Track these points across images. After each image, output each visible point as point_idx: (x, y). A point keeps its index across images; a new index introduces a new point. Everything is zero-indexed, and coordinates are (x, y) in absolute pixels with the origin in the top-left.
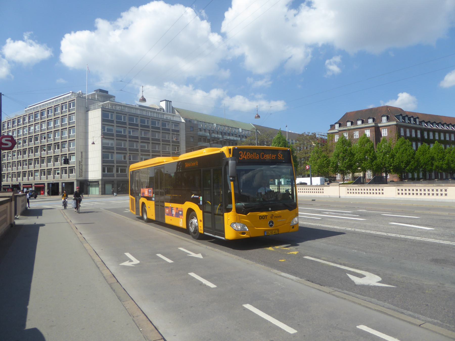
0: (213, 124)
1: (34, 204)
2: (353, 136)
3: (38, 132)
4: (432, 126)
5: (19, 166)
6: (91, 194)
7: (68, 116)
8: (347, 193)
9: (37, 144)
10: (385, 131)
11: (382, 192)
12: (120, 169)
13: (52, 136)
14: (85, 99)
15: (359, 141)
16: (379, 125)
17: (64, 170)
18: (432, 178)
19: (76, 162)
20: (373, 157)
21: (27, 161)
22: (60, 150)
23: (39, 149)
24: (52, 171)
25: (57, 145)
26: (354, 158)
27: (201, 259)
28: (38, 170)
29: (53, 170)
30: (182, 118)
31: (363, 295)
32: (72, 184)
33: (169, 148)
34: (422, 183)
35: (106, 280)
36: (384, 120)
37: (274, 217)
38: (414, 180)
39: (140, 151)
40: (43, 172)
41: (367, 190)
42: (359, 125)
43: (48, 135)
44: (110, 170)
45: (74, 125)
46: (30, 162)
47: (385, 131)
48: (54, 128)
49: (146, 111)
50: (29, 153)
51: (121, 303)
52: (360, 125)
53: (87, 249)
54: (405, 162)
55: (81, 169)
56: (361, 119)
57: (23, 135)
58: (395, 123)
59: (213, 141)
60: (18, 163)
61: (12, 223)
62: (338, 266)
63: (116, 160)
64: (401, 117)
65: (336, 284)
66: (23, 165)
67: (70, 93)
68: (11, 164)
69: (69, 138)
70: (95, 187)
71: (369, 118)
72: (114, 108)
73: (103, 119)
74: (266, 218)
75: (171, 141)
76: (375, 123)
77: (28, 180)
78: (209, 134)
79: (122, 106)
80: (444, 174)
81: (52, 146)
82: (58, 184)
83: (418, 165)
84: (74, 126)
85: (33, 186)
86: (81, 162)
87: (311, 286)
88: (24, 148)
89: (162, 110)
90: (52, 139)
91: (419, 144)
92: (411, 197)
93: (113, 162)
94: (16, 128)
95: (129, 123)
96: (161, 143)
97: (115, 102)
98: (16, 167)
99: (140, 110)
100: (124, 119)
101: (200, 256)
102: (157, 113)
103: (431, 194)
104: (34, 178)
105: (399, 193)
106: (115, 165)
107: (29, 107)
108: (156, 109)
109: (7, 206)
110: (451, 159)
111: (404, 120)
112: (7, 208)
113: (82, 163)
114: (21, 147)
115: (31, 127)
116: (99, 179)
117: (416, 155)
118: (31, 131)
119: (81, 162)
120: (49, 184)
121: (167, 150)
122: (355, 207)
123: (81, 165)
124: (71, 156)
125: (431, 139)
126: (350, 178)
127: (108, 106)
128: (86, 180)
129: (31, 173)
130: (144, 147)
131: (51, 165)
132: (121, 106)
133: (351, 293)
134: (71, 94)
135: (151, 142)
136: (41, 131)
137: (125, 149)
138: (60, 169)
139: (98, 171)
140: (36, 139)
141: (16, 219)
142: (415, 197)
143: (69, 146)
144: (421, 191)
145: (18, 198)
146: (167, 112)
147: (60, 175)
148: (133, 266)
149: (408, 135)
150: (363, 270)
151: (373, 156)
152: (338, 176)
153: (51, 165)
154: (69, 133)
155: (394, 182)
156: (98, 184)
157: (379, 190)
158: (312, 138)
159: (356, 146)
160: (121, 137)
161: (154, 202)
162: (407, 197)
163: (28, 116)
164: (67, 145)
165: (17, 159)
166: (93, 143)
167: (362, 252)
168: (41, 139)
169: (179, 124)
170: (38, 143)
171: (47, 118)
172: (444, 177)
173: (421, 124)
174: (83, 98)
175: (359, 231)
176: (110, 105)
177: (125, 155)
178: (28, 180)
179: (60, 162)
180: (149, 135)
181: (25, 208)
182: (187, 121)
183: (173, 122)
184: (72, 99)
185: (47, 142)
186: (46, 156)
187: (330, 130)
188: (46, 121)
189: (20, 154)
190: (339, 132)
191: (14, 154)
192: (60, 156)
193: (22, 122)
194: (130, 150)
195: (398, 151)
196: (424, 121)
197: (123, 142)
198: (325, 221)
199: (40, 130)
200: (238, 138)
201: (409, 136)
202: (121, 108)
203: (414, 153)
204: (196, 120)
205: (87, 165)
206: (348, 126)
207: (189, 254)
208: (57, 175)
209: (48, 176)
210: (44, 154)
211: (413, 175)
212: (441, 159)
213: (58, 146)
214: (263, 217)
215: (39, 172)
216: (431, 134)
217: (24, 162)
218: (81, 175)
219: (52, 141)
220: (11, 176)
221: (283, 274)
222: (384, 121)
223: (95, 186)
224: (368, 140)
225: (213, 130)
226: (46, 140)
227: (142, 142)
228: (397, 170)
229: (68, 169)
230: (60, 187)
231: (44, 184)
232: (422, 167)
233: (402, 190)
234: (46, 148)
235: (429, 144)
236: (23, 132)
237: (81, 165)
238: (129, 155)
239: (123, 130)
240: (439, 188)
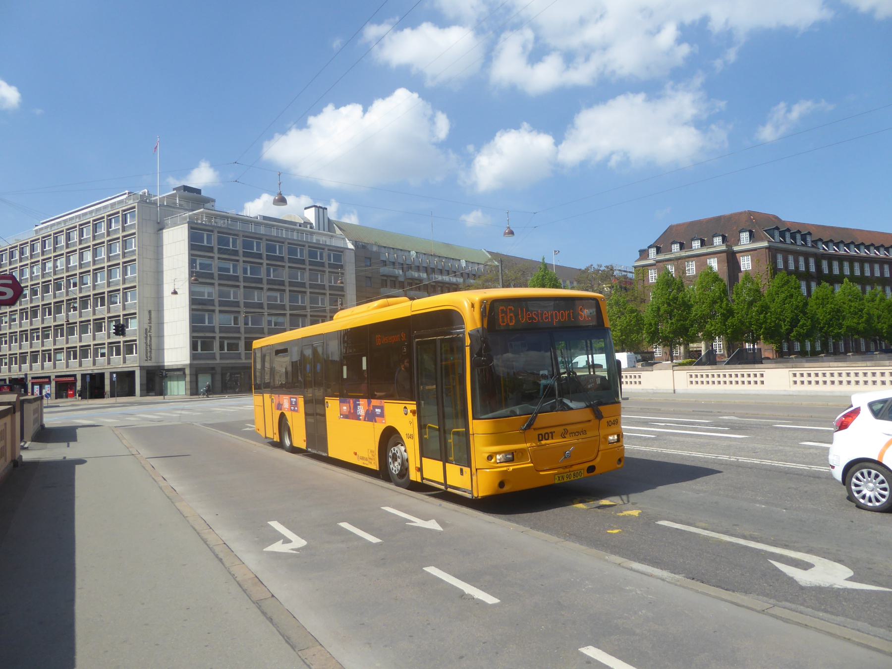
0: (409, 252)
1: (52, 419)
2: (684, 272)
3: (61, 272)
4: (836, 249)
5: (23, 342)
6: (169, 393)
7: (121, 240)
8: (689, 383)
9: (59, 297)
10: (746, 260)
11: (762, 379)
12: (228, 344)
13: (89, 279)
14: (154, 206)
15: (698, 280)
16: (736, 248)
17: (115, 348)
18: (839, 350)
19: (138, 332)
20: (728, 311)
21: (40, 331)
22: (106, 307)
23: (64, 307)
24: (90, 349)
25: (100, 298)
26: (690, 313)
27: (440, 533)
28: (63, 349)
29: (92, 347)
30: (348, 241)
31: (832, 613)
32: (132, 374)
33: (323, 300)
34: (823, 362)
35: (245, 591)
36: (745, 239)
37: (568, 433)
38: (812, 355)
39: (265, 306)
40: (71, 352)
41: (719, 376)
43: (81, 278)
44: (206, 345)
45: (133, 258)
46: (46, 333)
47: (746, 260)
48: (94, 264)
49: (278, 228)
50: (44, 314)
51: (295, 652)
52: (698, 249)
53: (185, 516)
54: (788, 322)
55: (149, 344)
56: (699, 238)
57: (32, 280)
58: (765, 244)
59: (410, 284)
60: (21, 336)
61: (16, 458)
62: (742, 542)
63: (220, 327)
64: (777, 233)
65: (756, 586)
66: (32, 338)
67: (125, 194)
68: (8, 337)
69: (124, 283)
70: (178, 381)
71: (715, 236)
72: (213, 224)
73: (191, 244)
75: (327, 287)
76: (727, 246)
77: (43, 368)
78: (403, 271)
79: (229, 220)
80: (862, 341)
81: (90, 299)
82: (102, 375)
83: (813, 327)
84: (134, 260)
85: (52, 380)
86: (149, 332)
87: (713, 594)
88: (33, 305)
89: (309, 226)
90: (90, 287)
91: (813, 285)
92: (821, 388)
93: (212, 330)
94: (18, 265)
95: (243, 251)
96: (308, 290)
97: (215, 211)
98: (18, 344)
99: (266, 225)
100: (234, 244)
101: (433, 525)
102: (298, 231)
103: (845, 383)
104: (55, 364)
105: (750, 381)
106: (218, 335)
107: (43, 223)
108: (298, 223)
109: (5, 424)
110: (876, 312)
111: (784, 238)
112: (6, 427)
113: (150, 334)
114: (28, 303)
115: (47, 264)
117: (809, 306)
118: (47, 271)
119: (148, 331)
120: (84, 376)
121: (320, 305)
122: (712, 412)
123: (149, 339)
124: (128, 318)
125: (836, 275)
126: (680, 353)
127: (202, 218)
128: (159, 367)
129: (47, 355)
131: (88, 339)
132: (227, 217)
133: (802, 607)
134: (126, 196)
135: (287, 289)
136: (67, 271)
137: (237, 304)
138: (106, 346)
139: (184, 347)
140: (58, 287)
141: (23, 448)
142: (829, 388)
143: (125, 299)
144: (826, 376)
145: (26, 406)
146: (319, 230)
147: (106, 358)
148: (295, 552)
149: (792, 267)
150: (800, 551)
151: (728, 308)
152: (659, 351)
153: (88, 339)
154: (125, 273)
155: (769, 361)
156: (184, 373)
157: (743, 376)
158: (607, 276)
159: (693, 290)
160: (228, 279)
162: (813, 388)
163: (40, 241)
164: (120, 299)
165: (21, 326)
166: (175, 293)
167: (779, 509)
168: (68, 286)
169: (342, 252)
170: (62, 295)
171: (80, 243)
172: (863, 348)
173: (816, 244)
174: (151, 203)
175: (747, 462)
176: (204, 217)
177: (236, 315)
178: (43, 368)
179: (106, 332)
180: (285, 275)
181: (39, 425)
182: (358, 246)
183: (331, 248)
184: (129, 207)
185: (66, 296)
186: (78, 320)
187: (638, 260)
188: (78, 251)
189: (24, 317)
190: (657, 264)
191: (13, 317)
192: (106, 320)
193: (28, 254)
194: (247, 305)
195: (775, 299)
196: (820, 240)
197: (232, 291)
198: (665, 441)
199: (65, 269)
200: (458, 279)
201: (793, 269)
202: (228, 222)
203: (805, 301)
204: (375, 244)
205: (160, 336)
206: (675, 252)
207: (410, 522)
208: (99, 358)
209: (82, 360)
210: (74, 316)
211: (803, 346)
212: (856, 314)
213: (103, 299)
214: (547, 435)
215: (63, 352)
216: (836, 265)
217: (34, 333)
218: (148, 358)
219: (90, 290)
220: (7, 361)
221: (636, 565)
222: (745, 241)
223: (178, 378)
224: (716, 279)
225: (410, 264)
226: (77, 288)
227: (269, 289)
228: (772, 335)
229: (123, 345)
230: (107, 382)
231: (75, 376)
232: (822, 328)
233: (809, 375)
234: (77, 305)
235: (832, 284)
236: (32, 273)
237: (149, 339)
238: (246, 316)
239: (231, 267)
240: (878, 370)
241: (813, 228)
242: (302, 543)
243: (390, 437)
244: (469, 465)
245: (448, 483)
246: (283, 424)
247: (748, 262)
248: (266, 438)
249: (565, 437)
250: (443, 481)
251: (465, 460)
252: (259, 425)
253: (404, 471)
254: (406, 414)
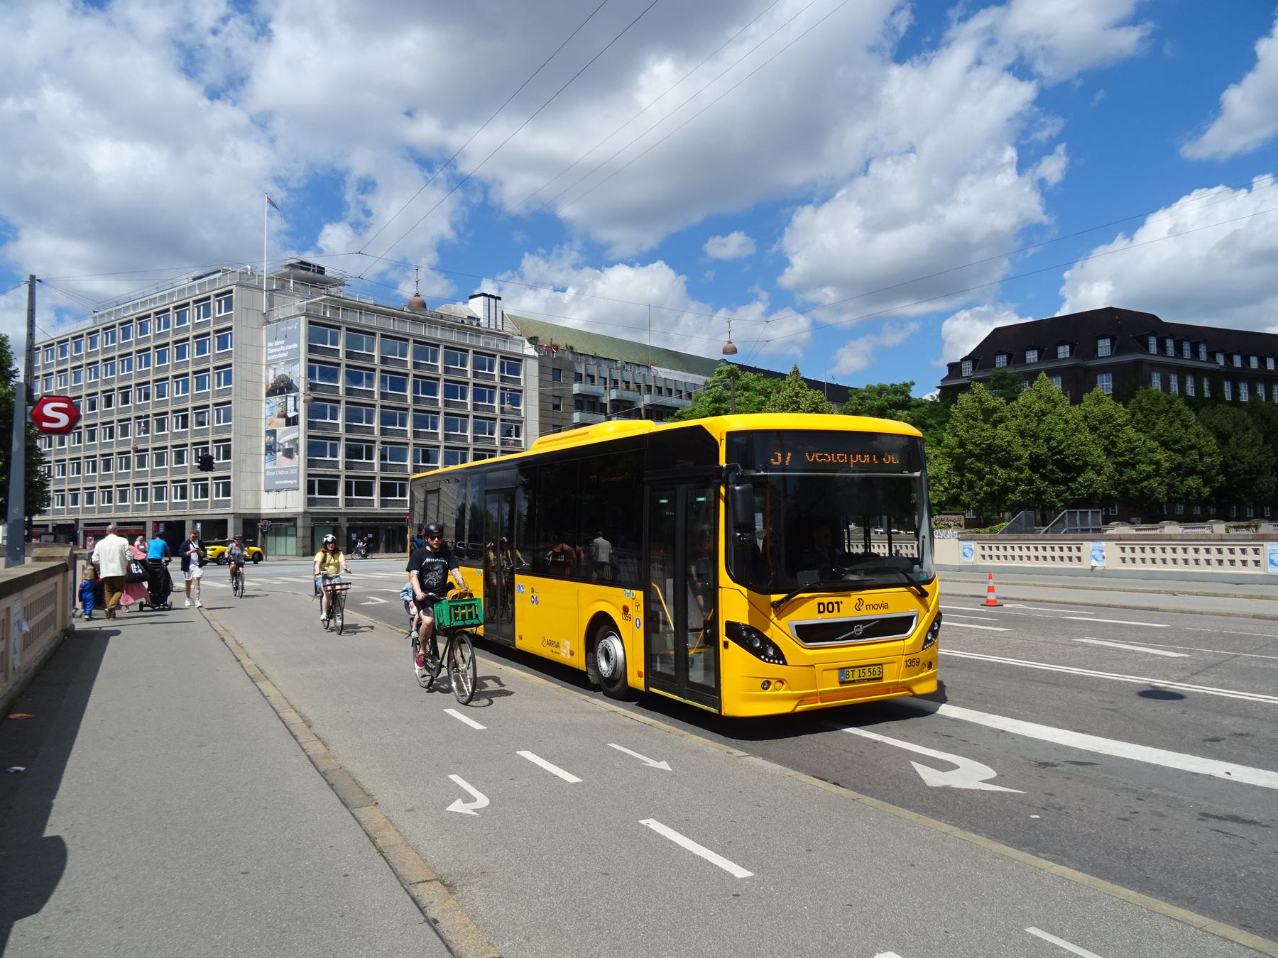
42: (1031, 364)
74: (839, 611)
89: (475, 323)
109: (56, 583)
116: (298, 514)
130: (489, 343)
144: (1234, 554)
169: (520, 361)
184: (223, 290)
214: (830, 605)
231: (144, 524)
243: (601, 626)
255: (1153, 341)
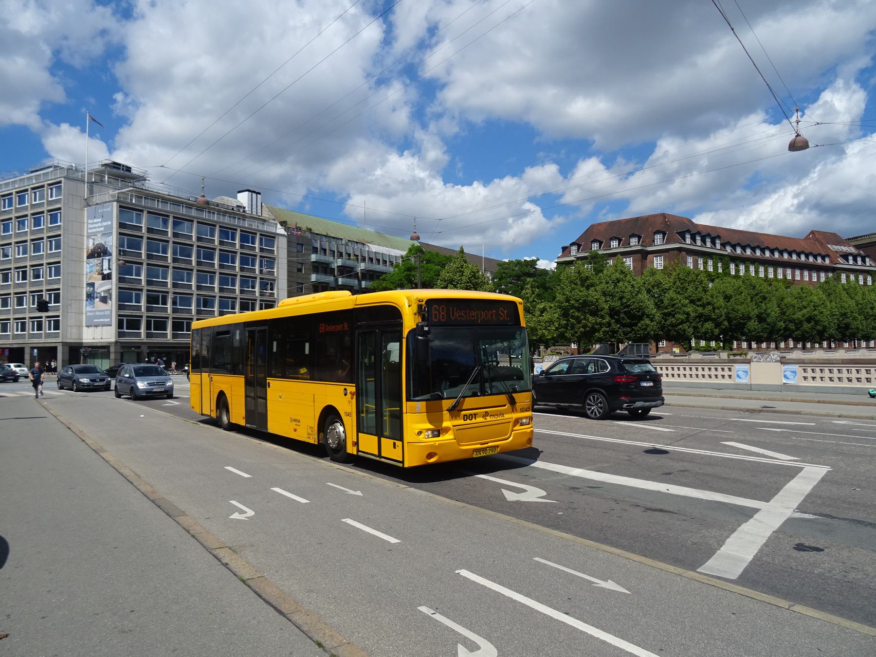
10: (659, 260)
36: (659, 240)
47: (659, 260)
89: (241, 210)
116: (111, 343)
130: (252, 225)
144: (731, 371)
156: (109, 352)
161: (114, 392)
184: (54, 181)
214: (471, 416)
241: (724, 232)
242: (251, 513)
243: (329, 415)
244: (401, 439)
245: (383, 455)
246: (222, 401)
247: (661, 262)
248: (202, 414)
249: (486, 412)
250: (376, 453)
251: (398, 434)
252: (195, 402)
253: (342, 445)
254: (346, 395)
255: (688, 236)
